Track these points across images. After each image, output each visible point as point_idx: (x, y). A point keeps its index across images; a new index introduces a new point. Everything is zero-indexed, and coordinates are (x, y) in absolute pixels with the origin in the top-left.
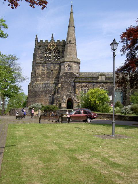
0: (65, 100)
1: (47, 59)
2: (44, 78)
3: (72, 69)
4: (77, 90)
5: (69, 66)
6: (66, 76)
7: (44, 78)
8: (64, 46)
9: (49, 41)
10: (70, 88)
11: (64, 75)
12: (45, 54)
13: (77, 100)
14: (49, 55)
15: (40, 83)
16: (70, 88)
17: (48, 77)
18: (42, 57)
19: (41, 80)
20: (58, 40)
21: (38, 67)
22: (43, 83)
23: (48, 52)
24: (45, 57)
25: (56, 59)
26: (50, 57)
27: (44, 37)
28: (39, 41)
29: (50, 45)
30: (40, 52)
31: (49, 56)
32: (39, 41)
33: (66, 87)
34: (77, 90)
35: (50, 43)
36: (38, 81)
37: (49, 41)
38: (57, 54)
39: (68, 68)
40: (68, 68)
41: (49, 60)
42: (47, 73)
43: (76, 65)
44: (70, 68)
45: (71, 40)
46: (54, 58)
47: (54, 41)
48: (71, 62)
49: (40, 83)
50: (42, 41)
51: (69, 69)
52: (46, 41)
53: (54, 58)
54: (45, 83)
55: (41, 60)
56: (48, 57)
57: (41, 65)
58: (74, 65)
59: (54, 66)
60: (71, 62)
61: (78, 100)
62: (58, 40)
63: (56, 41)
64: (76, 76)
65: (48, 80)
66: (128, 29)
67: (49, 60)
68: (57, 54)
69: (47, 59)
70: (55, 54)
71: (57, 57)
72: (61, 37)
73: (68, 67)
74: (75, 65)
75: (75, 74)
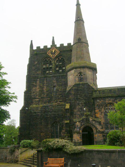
0: (80, 129)
1: (47, 72)
2: (43, 98)
3: (86, 78)
4: (98, 110)
5: (81, 74)
6: (77, 90)
7: (43, 98)
8: (97, 142)
9: (49, 46)
10: (85, 109)
11: (74, 88)
12: (44, 64)
13: (99, 127)
14: (49, 65)
15: (37, 106)
16: (85, 109)
17: (49, 97)
18: (38, 69)
19: (39, 101)
20: (62, 45)
21: (34, 84)
22: (42, 105)
23: (48, 62)
24: (44, 68)
25: (61, 71)
26: (51, 68)
27: (43, 42)
28: (35, 48)
29: (50, 51)
30: (36, 62)
31: (50, 66)
32: (35, 48)
33: (78, 107)
34: (98, 110)
35: (49, 49)
36: (35, 104)
37: (49, 46)
38: (61, 63)
39: (80, 77)
40: (80, 77)
41: (49, 73)
42: (47, 91)
43: (92, 73)
44: (82, 77)
45: (81, 37)
46: (58, 69)
47: (56, 45)
48: (84, 67)
49: (37, 106)
50: (46, 46)
51: (81, 80)
52: (68, 44)
53: (58, 69)
54: (45, 106)
55: (38, 72)
56: (47, 68)
57: (38, 80)
58: (89, 73)
59: (57, 80)
60: (84, 67)
61: (102, 128)
62: (62, 45)
63: (58, 46)
64: (93, 88)
65: (49, 102)
66: (65, 45)
67: (49, 73)
68: (61, 63)
69: (47, 72)
70: (58, 64)
71: (60, 68)
72: (66, 38)
73: (80, 76)
74: (90, 73)
75: (91, 86)
